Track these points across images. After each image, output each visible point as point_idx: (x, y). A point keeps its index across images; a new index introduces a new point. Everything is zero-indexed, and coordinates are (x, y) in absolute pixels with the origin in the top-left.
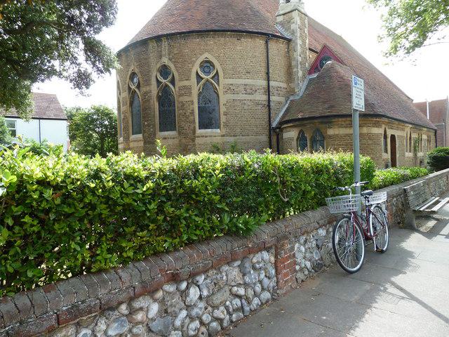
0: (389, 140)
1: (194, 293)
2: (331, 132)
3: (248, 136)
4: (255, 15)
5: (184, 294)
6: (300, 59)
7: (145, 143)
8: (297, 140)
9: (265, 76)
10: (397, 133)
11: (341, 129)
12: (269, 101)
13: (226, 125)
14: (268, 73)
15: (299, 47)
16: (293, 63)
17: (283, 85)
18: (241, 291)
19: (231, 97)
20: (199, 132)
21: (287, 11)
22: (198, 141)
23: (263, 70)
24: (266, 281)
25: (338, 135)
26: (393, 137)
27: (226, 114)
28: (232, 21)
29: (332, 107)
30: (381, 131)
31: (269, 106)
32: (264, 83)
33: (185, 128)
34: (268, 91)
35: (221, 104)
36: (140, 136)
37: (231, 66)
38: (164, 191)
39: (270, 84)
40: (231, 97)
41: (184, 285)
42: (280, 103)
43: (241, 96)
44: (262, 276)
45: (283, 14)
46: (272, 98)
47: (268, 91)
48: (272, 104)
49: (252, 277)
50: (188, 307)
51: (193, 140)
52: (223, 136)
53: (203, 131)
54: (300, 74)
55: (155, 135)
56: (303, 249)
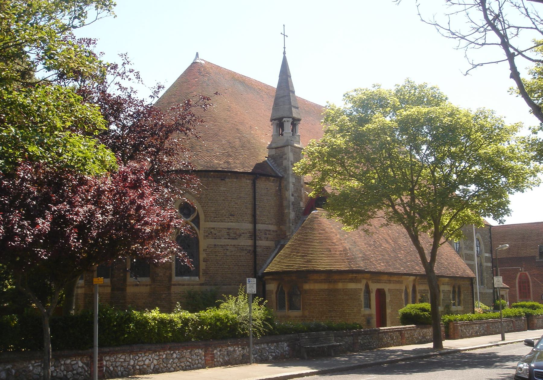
0: (373, 296)
1: (175, 355)
2: (307, 287)
3: (230, 285)
4: (243, 147)
5: (172, 355)
6: (292, 199)
7: (113, 290)
8: (276, 293)
9: (249, 218)
10: (386, 287)
11: (316, 284)
12: (255, 246)
13: (206, 273)
14: (254, 216)
15: (291, 186)
16: (285, 203)
17: (272, 228)
18: (190, 360)
19: (211, 241)
20: (176, 279)
21: (279, 145)
22: (174, 289)
23: (249, 212)
24: (200, 360)
25: (313, 290)
26: (381, 294)
27: (205, 260)
28: (217, 157)
29: (309, 261)
30: (361, 286)
31: (255, 252)
32: (250, 226)
33: (160, 274)
34: (254, 235)
35: (201, 249)
36: (108, 281)
37: (213, 209)
38: (457, 164)
39: (257, 227)
40: (211, 241)
41: (172, 352)
42: (268, 248)
43: (223, 242)
44: (199, 358)
45: (275, 148)
46: (259, 243)
47: (254, 235)
48: (259, 250)
49: (194, 357)
50: (173, 359)
51: (169, 288)
52: (202, 284)
53: (179, 278)
54: (292, 215)
55: (125, 280)
56: (219, 353)
